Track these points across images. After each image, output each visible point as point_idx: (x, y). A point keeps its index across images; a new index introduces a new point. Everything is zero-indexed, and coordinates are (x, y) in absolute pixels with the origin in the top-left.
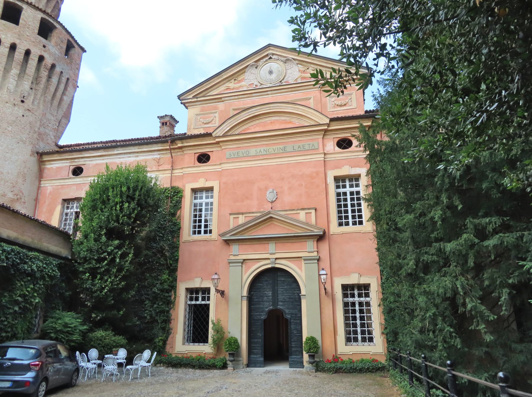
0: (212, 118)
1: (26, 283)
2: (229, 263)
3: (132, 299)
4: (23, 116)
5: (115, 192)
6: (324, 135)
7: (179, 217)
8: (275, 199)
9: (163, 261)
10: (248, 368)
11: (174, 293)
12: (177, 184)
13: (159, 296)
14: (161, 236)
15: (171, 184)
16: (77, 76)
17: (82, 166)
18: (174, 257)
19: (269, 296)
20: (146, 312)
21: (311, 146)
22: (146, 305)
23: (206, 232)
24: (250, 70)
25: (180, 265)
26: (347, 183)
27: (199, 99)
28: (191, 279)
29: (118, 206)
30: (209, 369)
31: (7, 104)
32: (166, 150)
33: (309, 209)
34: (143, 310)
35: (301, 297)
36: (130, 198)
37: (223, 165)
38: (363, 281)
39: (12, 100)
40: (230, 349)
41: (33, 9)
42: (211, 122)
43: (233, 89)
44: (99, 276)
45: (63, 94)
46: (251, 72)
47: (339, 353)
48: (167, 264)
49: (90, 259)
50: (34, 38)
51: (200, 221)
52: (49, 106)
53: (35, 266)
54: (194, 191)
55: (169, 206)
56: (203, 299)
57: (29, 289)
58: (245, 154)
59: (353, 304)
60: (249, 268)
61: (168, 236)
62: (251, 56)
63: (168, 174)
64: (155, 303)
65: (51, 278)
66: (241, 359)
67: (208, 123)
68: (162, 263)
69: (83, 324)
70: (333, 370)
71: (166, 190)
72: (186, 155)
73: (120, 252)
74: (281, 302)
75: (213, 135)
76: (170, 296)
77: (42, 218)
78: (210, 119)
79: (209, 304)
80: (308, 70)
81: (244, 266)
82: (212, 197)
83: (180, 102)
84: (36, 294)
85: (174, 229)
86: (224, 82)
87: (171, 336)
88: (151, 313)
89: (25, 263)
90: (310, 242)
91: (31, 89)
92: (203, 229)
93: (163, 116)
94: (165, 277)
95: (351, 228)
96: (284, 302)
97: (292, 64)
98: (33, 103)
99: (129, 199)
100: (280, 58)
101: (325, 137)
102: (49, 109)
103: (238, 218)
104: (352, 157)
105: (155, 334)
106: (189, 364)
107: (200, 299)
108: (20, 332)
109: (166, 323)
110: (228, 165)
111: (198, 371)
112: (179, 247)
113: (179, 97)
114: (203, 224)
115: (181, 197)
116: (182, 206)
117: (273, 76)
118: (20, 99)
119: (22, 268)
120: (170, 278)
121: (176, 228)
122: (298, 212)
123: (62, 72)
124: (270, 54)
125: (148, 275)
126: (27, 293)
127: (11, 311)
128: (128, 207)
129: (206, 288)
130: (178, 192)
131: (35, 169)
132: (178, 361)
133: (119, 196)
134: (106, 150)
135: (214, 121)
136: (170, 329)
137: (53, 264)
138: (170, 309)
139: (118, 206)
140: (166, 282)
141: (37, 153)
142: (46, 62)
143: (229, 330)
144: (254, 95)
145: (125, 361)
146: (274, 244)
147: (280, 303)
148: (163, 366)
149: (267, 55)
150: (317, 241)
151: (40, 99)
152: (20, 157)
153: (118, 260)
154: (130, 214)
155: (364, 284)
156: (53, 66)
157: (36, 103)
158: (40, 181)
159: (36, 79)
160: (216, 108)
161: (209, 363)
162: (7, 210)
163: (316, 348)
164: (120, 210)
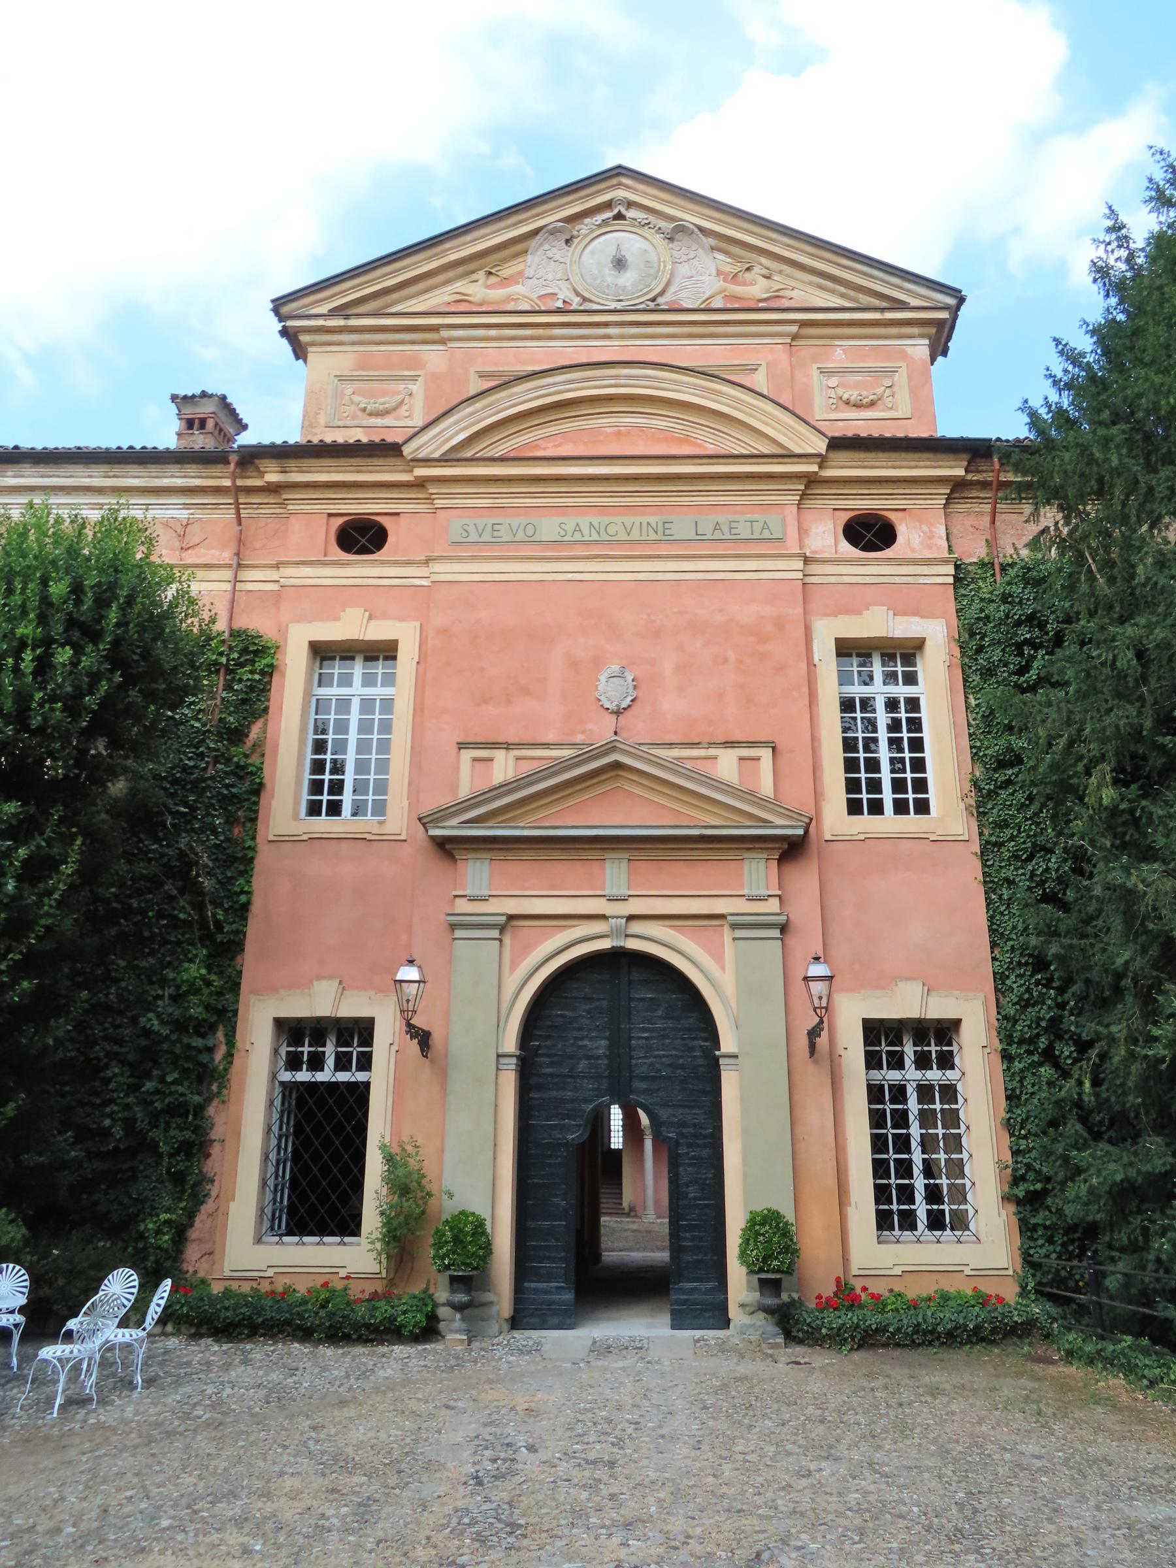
0: (400, 398)
2: (453, 927)
3: (60, 1054)
5: (17, 599)
6: (804, 495)
8: (627, 702)
9: (189, 908)
10: (517, 1334)
11: (226, 1035)
12: (255, 622)
13: (165, 1046)
14: (184, 814)
15: (231, 619)
18: (232, 895)
19: (598, 1058)
20: (108, 1110)
21: (758, 527)
22: (109, 1080)
24: (546, 247)
25: (254, 928)
26: (877, 669)
27: (353, 322)
28: (302, 984)
29: (28, 656)
30: (372, 1341)
33: (752, 744)
35: (722, 1061)
37: (436, 567)
38: (938, 1009)
40: (459, 1260)
42: (394, 409)
43: (481, 304)
47: (855, 1272)
48: (203, 922)
54: (322, 652)
55: (218, 701)
56: (342, 1063)
58: (521, 531)
59: (899, 1093)
60: (527, 949)
61: (208, 814)
62: (555, 198)
64: (147, 1075)
66: (490, 1297)
67: (387, 412)
68: (182, 916)
70: (853, 1338)
72: (293, 519)
73: (22, 852)
74: (644, 1078)
75: (407, 450)
76: (210, 1050)
78: (392, 401)
79: (367, 1085)
80: (747, 275)
81: (507, 940)
82: (389, 680)
83: (279, 326)
86: (451, 274)
88: (126, 1114)
90: (754, 862)
93: (194, 396)
95: (889, 822)
96: (654, 1078)
97: (694, 246)
99: (76, 635)
100: (652, 219)
101: (808, 503)
103: (491, 760)
104: (897, 580)
105: (143, 1201)
106: (288, 1322)
107: (330, 1062)
109: (189, 1156)
110: (457, 567)
111: (327, 1352)
112: (252, 859)
113: (279, 305)
115: (269, 672)
116: (273, 705)
117: (628, 279)
120: (213, 977)
122: (712, 752)
124: (620, 202)
125: (122, 963)
128: (75, 663)
129: (356, 1021)
130: (256, 653)
133: (32, 616)
135: (405, 407)
136: (205, 1180)
138: (209, 1100)
140: (197, 992)
143: (448, 1182)
144: (557, 332)
145: (20, 1318)
146: (624, 864)
147: (639, 1085)
149: (608, 205)
150: (781, 861)
154: (78, 694)
155: (939, 1021)
160: (415, 363)
161: (372, 1316)
163: (787, 1253)
164: (35, 673)
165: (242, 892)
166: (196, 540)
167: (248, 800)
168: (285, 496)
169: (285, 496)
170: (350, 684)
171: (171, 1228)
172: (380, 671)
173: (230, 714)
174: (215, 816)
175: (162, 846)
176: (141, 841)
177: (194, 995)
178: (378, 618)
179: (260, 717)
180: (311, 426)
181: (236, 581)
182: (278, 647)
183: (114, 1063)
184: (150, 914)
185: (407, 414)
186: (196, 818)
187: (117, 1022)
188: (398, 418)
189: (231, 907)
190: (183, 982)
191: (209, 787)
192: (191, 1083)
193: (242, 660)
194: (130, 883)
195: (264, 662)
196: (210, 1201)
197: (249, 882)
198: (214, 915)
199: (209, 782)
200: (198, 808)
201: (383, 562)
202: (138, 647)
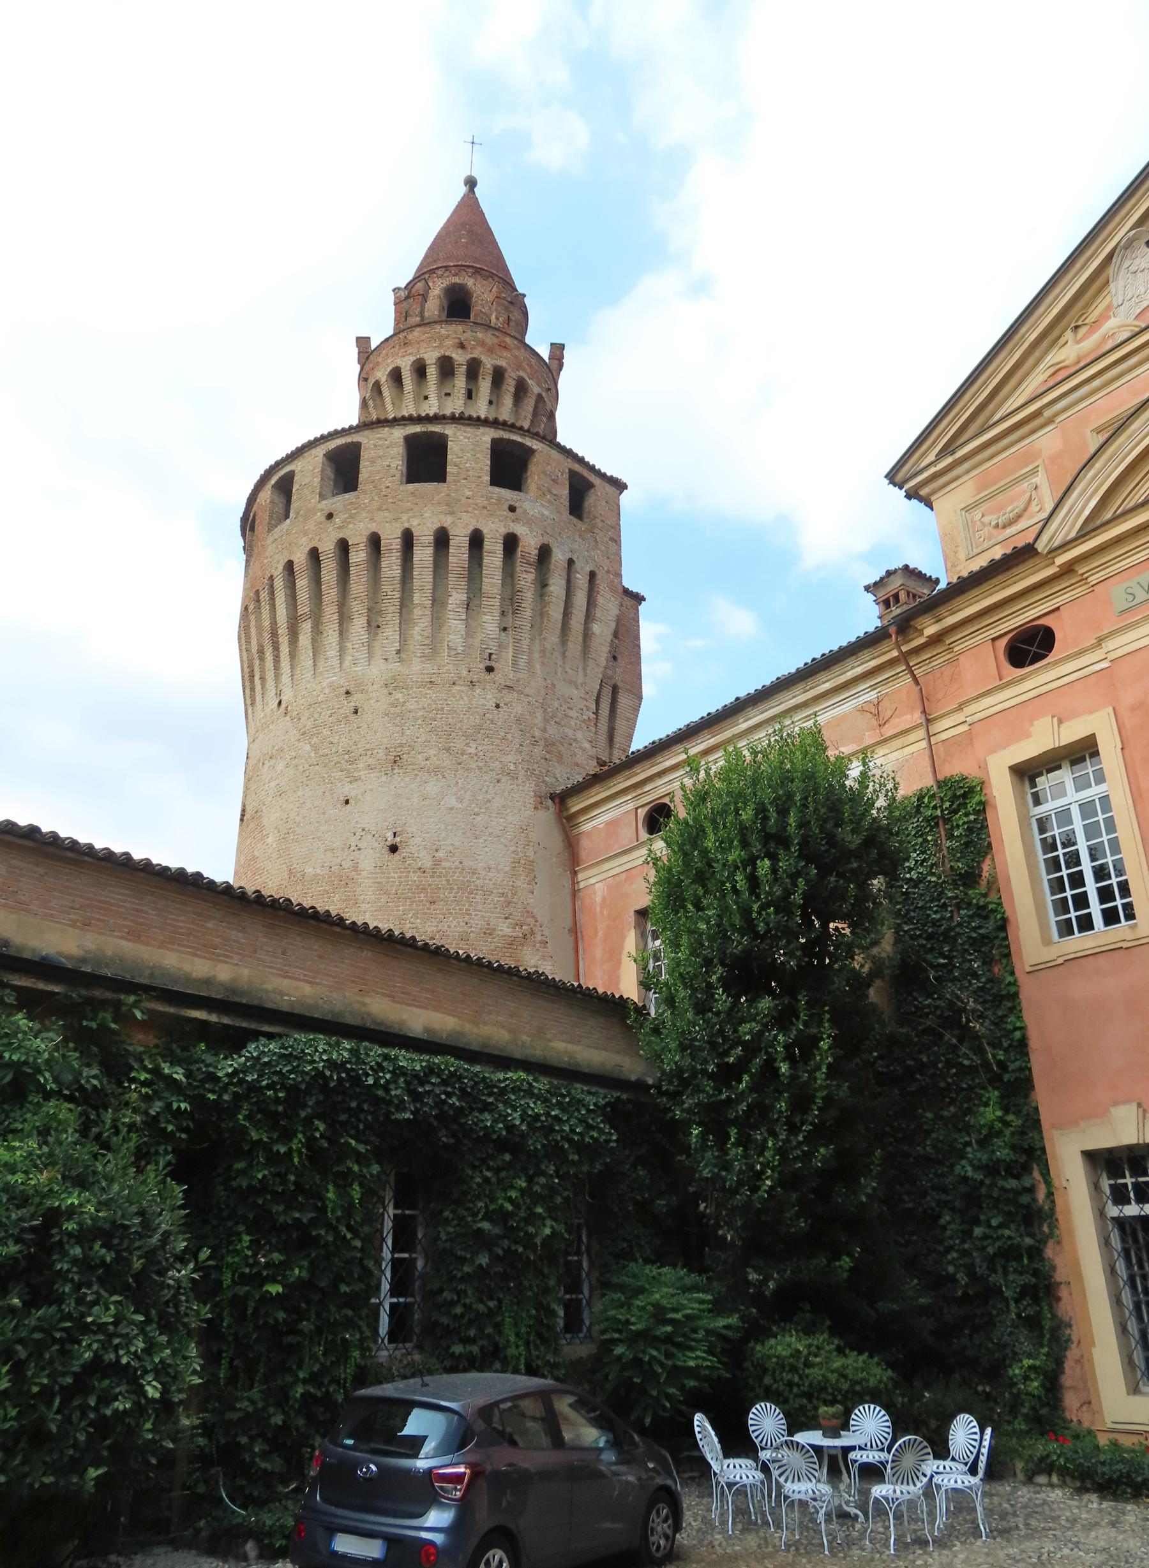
0: (1027, 496)
1: (503, 1174)
4: (498, 706)
7: (993, 883)
9: (971, 1055)
11: (1042, 1174)
12: (957, 767)
13: (983, 1191)
16: (616, 559)
17: (666, 800)
18: (1008, 1033)
20: (949, 1257)
23: (1110, 917)
24: (1127, 263)
25: (1037, 1063)
28: (1098, 1113)
31: (456, 688)
32: (892, 663)
34: (941, 1249)
36: (775, 841)
37: (1110, 644)
39: (464, 672)
41: (468, 429)
42: (1025, 510)
43: (1078, 362)
44: (733, 1132)
45: (589, 617)
46: (1133, 268)
48: (986, 1064)
49: (694, 1074)
50: (482, 497)
51: (1077, 880)
52: (560, 662)
53: (516, 1115)
55: (945, 852)
57: (513, 1194)
63: (916, 745)
64: (976, 1222)
65: (589, 1151)
67: (1019, 517)
68: (966, 1062)
69: (718, 1307)
71: (921, 798)
72: (962, 659)
75: (1041, 546)
76: (1031, 1190)
77: (596, 980)
78: (1020, 504)
82: (1100, 778)
83: (903, 493)
84: (539, 1210)
85: (982, 931)
86: (1037, 354)
87: (1073, 1353)
89: (486, 1108)
91: (505, 629)
92: (1095, 908)
93: (882, 579)
94: (991, 1113)
98: (515, 664)
102: (559, 670)
108: (512, 1339)
109: (1036, 1300)
113: (894, 477)
114: (1091, 887)
116: (994, 840)
118: (482, 666)
119: (476, 1124)
120: (1010, 1117)
121: (991, 925)
123: (571, 562)
125: (929, 1115)
126: (510, 1208)
127: (467, 1269)
128: (774, 870)
130: (965, 796)
131: (556, 841)
132: (1120, 1466)
133: (735, 843)
134: (715, 728)
135: (1034, 503)
137: (585, 1106)
138: (1044, 1241)
139: (738, 877)
140: (1000, 1134)
141: (552, 797)
142: (523, 547)
148: (1063, 1485)
151: (531, 651)
152: (510, 818)
153: (784, 1068)
154: (787, 894)
156: (545, 553)
157: (522, 663)
158: (575, 873)
159: (511, 603)
160: (1030, 456)
162: (410, 950)
165: (1016, 1029)
166: (889, 713)
167: (997, 937)
168: (948, 642)
169: (948, 642)
170: (1064, 794)
171: (1038, 1374)
172: (1090, 770)
173: (958, 861)
174: (971, 960)
175: (934, 999)
176: (916, 999)
177: (997, 1137)
178: (1068, 719)
179: (987, 854)
180: (953, 566)
181: (929, 736)
182: (983, 783)
183: (945, 1211)
184: (940, 1065)
185: (1038, 508)
186: (955, 967)
187: (940, 1171)
188: (1032, 516)
189: (1010, 1046)
190: (982, 1126)
191: (959, 934)
192: (1019, 1225)
193: (955, 806)
194: (916, 1039)
195: (974, 801)
196: (1074, 1346)
197: (1019, 1018)
198: (994, 1056)
199: (957, 930)
200: (955, 957)
201: (1056, 663)
202: (822, 839)
